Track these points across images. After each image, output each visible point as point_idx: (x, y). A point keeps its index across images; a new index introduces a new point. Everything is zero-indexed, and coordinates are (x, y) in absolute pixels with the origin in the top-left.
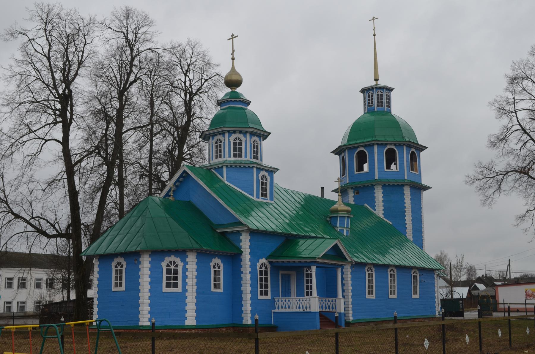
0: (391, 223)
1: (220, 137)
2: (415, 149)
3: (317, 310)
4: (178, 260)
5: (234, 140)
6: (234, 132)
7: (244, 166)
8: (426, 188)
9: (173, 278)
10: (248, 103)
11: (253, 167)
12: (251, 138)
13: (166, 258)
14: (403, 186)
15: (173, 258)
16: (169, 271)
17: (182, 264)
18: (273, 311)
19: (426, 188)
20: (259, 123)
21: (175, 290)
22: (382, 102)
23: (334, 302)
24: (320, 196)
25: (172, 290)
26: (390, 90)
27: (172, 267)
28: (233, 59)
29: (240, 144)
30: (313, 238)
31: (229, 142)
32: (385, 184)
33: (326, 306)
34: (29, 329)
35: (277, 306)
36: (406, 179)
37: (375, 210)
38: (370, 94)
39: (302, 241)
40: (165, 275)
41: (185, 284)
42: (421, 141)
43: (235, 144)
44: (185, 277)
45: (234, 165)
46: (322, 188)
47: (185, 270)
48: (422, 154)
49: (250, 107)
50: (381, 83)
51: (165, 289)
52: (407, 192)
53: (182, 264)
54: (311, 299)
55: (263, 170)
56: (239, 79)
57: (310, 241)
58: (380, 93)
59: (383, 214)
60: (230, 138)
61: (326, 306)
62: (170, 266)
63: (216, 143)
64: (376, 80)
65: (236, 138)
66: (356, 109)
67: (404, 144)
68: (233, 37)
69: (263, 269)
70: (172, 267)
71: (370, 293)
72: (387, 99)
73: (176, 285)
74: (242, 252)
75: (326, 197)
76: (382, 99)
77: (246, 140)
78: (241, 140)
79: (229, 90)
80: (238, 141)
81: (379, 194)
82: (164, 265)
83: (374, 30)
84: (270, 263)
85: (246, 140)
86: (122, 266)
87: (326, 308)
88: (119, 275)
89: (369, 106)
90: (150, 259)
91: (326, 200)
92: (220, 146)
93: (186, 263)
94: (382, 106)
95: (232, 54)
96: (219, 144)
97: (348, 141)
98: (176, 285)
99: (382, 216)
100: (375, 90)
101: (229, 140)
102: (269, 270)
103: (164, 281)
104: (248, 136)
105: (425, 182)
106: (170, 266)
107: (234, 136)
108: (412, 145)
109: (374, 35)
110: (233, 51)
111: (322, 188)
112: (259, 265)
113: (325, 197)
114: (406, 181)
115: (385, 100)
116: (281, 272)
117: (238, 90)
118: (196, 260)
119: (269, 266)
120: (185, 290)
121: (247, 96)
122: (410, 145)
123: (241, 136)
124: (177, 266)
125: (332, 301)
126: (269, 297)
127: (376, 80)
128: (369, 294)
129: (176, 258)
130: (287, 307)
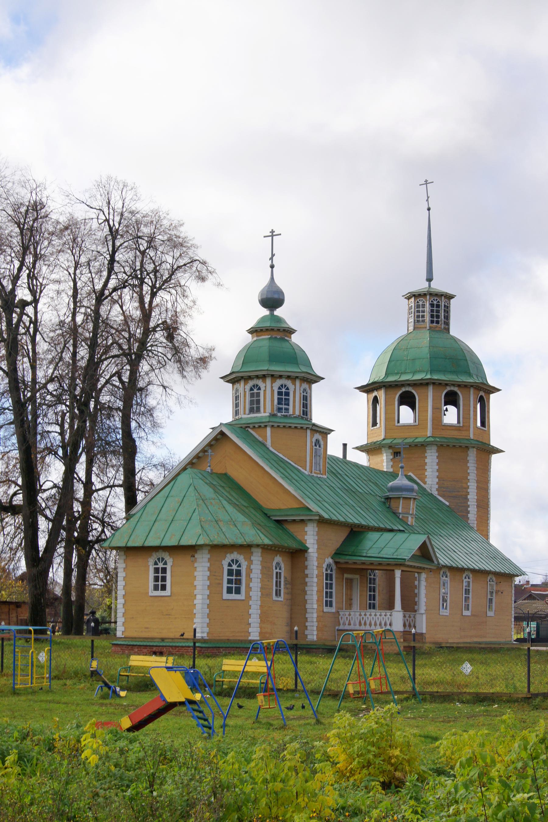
0: (447, 503)
1: (260, 383)
2: (484, 391)
3: (401, 629)
4: (241, 558)
5: (279, 388)
6: (281, 377)
7: (296, 427)
8: (497, 451)
9: (235, 583)
10: (290, 331)
11: (307, 428)
12: (301, 386)
13: (228, 555)
14: (467, 448)
15: (235, 555)
16: (230, 573)
17: (246, 563)
18: (337, 628)
19: (497, 451)
20: (308, 364)
21: (237, 597)
22: (438, 317)
23: (412, 618)
24: (341, 456)
25: (234, 596)
26: (449, 297)
27: (234, 567)
28: (272, 267)
29: (287, 394)
30: (391, 530)
31: (273, 391)
32: (442, 445)
33: (375, 622)
34: (265, 644)
35: (341, 622)
36: (472, 437)
37: (425, 483)
38: (421, 303)
39: (373, 536)
40: (226, 577)
41: (249, 588)
42: (492, 382)
43: (280, 393)
44: (249, 579)
45: (282, 425)
46: (345, 445)
47: (249, 571)
48: (492, 396)
49: (295, 338)
50: (438, 285)
51: (226, 596)
52: (472, 455)
53: (246, 563)
54: (393, 613)
55: (317, 431)
56: (281, 297)
57: (387, 536)
58: (435, 302)
59: (437, 490)
60: (274, 385)
61: (375, 622)
62: (231, 566)
63: (251, 389)
64: (430, 279)
65: (282, 386)
66: (399, 323)
67: (472, 386)
68: (273, 234)
69: (329, 572)
70: (234, 567)
71: (278, 593)
72: (445, 310)
73: (238, 591)
74: (308, 548)
75: (349, 458)
76: (438, 311)
77: (295, 389)
78: (288, 389)
79: (265, 312)
80: (284, 390)
81: (431, 458)
82: (225, 563)
83: (427, 200)
84: (336, 563)
85: (295, 389)
86: (165, 563)
87: (360, 624)
88: (160, 575)
89: (418, 321)
90: (209, 556)
91: (350, 462)
92: (258, 395)
93: (250, 562)
94: (438, 322)
95: (271, 259)
96: (255, 391)
97: (387, 374)
98: (238, 591)
99: (435, 493)
100: (428, 297)
101: (272, 387)
102: (334, 573)
103: (225, 585)
104: (298, 382)
105: (494, 442)
106: (231, 566)
107: (279, 382)
108: (481, 388)
109: (429, 209)
110: (273, 255)
111: (345, 445)
112: (325, 566)
113: (349, 458)
114: (473, 442)
115: (442, 314)
116: (346, 576)
117: (278, 312)
118: (260, 559)
119: (334, 567)
120: (248, 597)
121: (291, 323)
122: (479, 387)
123: (289, 383)
124: (239, 566)
125: (410, 617)
126: (333, 610)
127: (430, 279)
128: (276, 595)
129: (239, 556)
130: (347, 623)
